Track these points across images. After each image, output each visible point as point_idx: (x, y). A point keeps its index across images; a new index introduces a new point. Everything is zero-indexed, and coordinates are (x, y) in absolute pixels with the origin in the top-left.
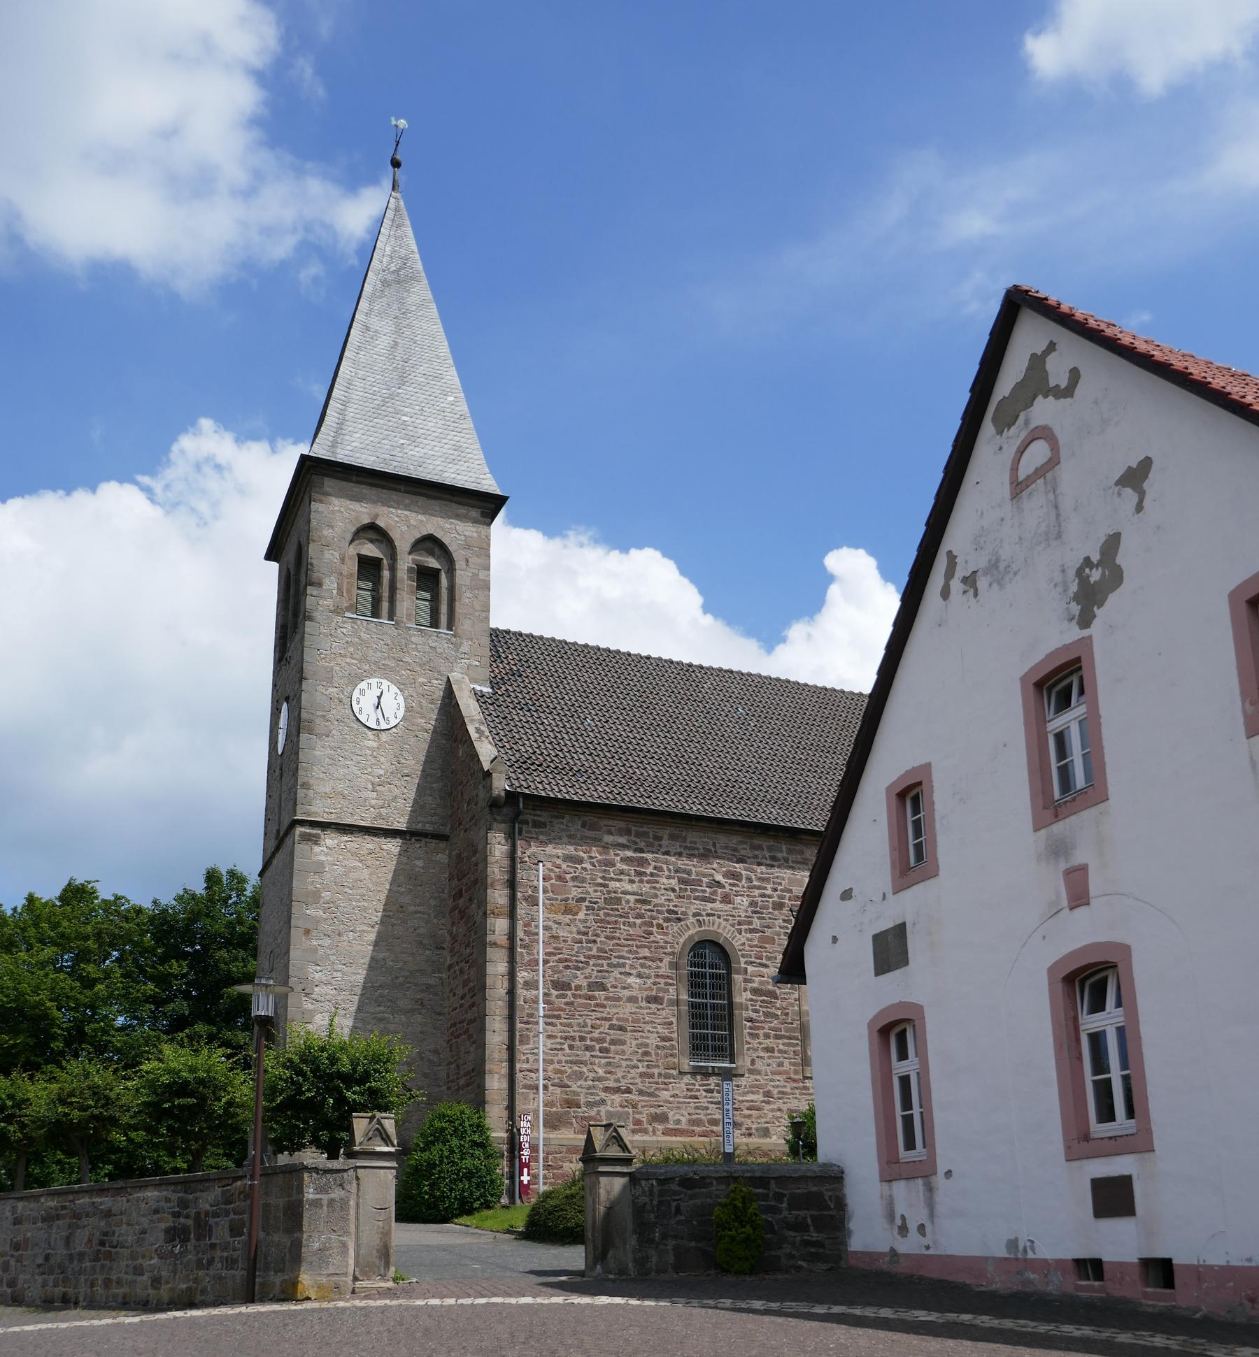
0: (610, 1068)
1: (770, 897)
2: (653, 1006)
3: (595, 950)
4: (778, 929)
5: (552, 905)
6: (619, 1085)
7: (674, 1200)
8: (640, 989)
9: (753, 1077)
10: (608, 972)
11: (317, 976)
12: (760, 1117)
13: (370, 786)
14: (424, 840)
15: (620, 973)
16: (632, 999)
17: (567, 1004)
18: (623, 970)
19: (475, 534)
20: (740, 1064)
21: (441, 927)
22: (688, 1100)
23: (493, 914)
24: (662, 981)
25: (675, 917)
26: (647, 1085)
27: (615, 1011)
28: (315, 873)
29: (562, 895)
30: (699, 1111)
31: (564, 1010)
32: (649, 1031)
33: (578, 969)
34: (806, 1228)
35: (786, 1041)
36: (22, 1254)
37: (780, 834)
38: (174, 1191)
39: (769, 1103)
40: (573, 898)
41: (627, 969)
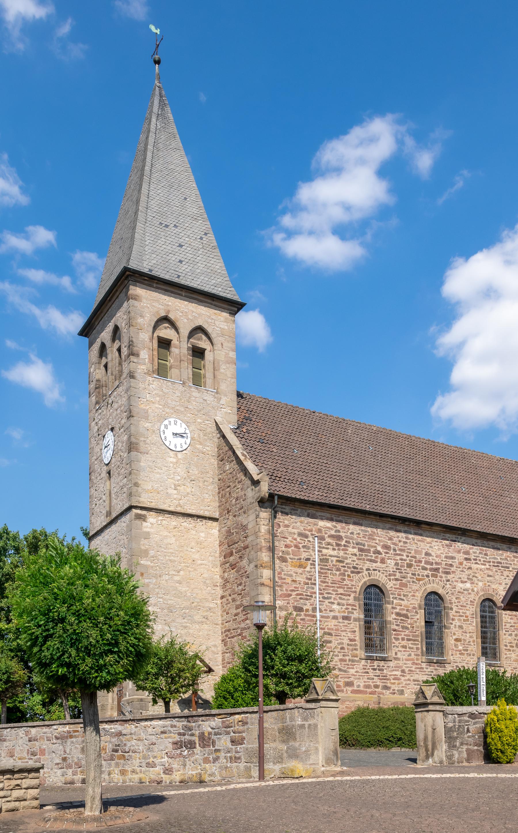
1: (405, 560)
2: (346, 621)
4: (409, 579)
5: (292, 562)
7: (466, 725)
8: (339, 612)
9: (396, 662)
12: (399, 684)
13: (173, 486)
14: (204, 521)
15: (329, 603)
16: (335, 618)
18: (330, 601)
19: (226, 327)
20: (390, 654)
21: (216, 573)
22: (363, 674)
23: (262, 566)
24: (350, 607)
25: (356, 571)
26: (343, 666)
28: (145, 538)
29: (297, 556)
30: (369, 680)
32: (344, 636)
33: (307, 599)
35: (412, 642)
36: (40, 758)
37: (412, 524)
39: (403, 676)
41: (332, 600)
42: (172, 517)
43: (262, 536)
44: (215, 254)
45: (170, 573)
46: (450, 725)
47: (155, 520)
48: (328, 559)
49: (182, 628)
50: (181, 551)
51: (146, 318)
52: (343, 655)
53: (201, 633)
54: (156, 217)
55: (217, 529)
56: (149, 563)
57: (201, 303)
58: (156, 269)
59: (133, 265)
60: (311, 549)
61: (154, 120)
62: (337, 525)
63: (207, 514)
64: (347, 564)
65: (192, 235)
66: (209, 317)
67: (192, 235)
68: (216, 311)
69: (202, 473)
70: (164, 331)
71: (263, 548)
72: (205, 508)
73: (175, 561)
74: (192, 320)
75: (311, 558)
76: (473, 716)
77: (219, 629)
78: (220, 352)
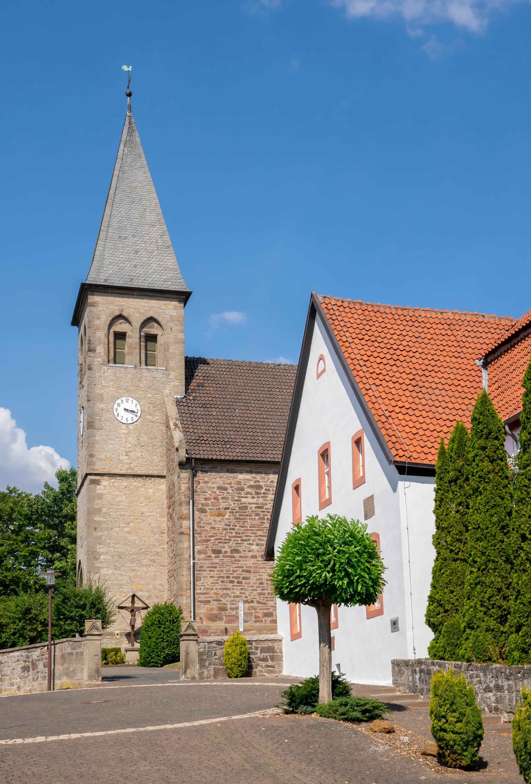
3: (234, 533)
5: (211, 512)
6: (247, 599)
8: (258, 551)
10: (241, 544)
11: (102, 550)
13: (124, 453)
14: (153, 479)
15: (248, 544)
16: (253, 557)
18: (249, 542)
19: (175, 314)
26: (262, 599)
27: (245, 563)
28: (98, 499)
32: (263, 572)
33: (225, 543)
34: (267, 661)
41: (251, 542)
42: (123, 478)
44: (169, 252)
46: (202, 650)
48: (247, 507)
52: (262, 590)
53: (148, 574)
54: (117, 232)
55: (165, 484)
56: (102, 519)
58: (111, 278)
59: (90, 280)
61: (122, 147)
62: (256, 476)
63: (155, 473)
64: (266, 509)
65: (148, 240)
66: (159, 308)
67: (148, 240)
68: (166, 302)
69: (151, 439)
70: (120, 326)
74: (143, 314)
76: (219, 643)
77: (165, 570)
78: (169, 336)
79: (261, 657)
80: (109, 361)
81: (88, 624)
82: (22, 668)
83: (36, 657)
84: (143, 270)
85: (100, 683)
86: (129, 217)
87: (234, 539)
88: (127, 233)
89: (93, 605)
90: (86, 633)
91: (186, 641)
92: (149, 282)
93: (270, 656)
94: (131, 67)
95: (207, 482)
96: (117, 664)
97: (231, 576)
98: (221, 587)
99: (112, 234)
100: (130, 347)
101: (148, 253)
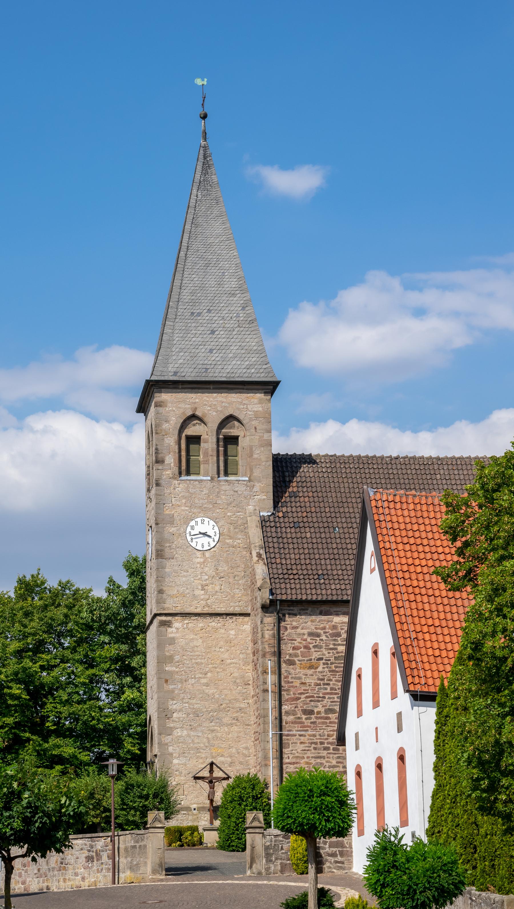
0: (339, 760)
3: (329, 689)
5: (301, 664)
11: (174, 707)
13: (200, 587)
14: (234, 618)
17: (311, 723)
19: (261, 409)
21: (247, 671)
28: (169, 644)
29: (306, 657)
31: (310, 727)
33: (319, 701)
34: (336, 856)
38: (88, 841)
40: (314, 659)
43: (266, 641)
44: (253, 329)
45: (197, 676)
46: (268, 844)
47: (181, 624)
49: (208, 732)
50: (209, 652)
51: (172, 422)
53: (230, 735)
54: (188, 307)
55: (249, 624)
56: (174, 669)
57: (232, 391)
58: (182, 370)
60: (324, 647)
63: (237, 610)
65: (227, 315)
67: (227, 315)
68: (249, 395)
69: (232, 568)
71: (267, 654)
72: (235, 605)
73: (202, 663)
74: (221, 411)
75: (324, 657)
78: (253, 437)
79: (330, 852)
80: (180, 474)
81: (151, 816)
82: (86, 858)
83: (100, 848)
84: (221, 355)
85: (164, 877)
86: (203, 285)
87: (329, 696)
88: (201, 308)
89: (156, 796)
90: (148, 826)
91: (252, 834)
92: (228, 371)
93: (339, 851)
94: (206, 80)
95: (296, 628)
96: (194, 845)
97: (326, 741)
98: (313, 755)
99: (182, 311)
100: (206, 454)
101: (226, 332)
